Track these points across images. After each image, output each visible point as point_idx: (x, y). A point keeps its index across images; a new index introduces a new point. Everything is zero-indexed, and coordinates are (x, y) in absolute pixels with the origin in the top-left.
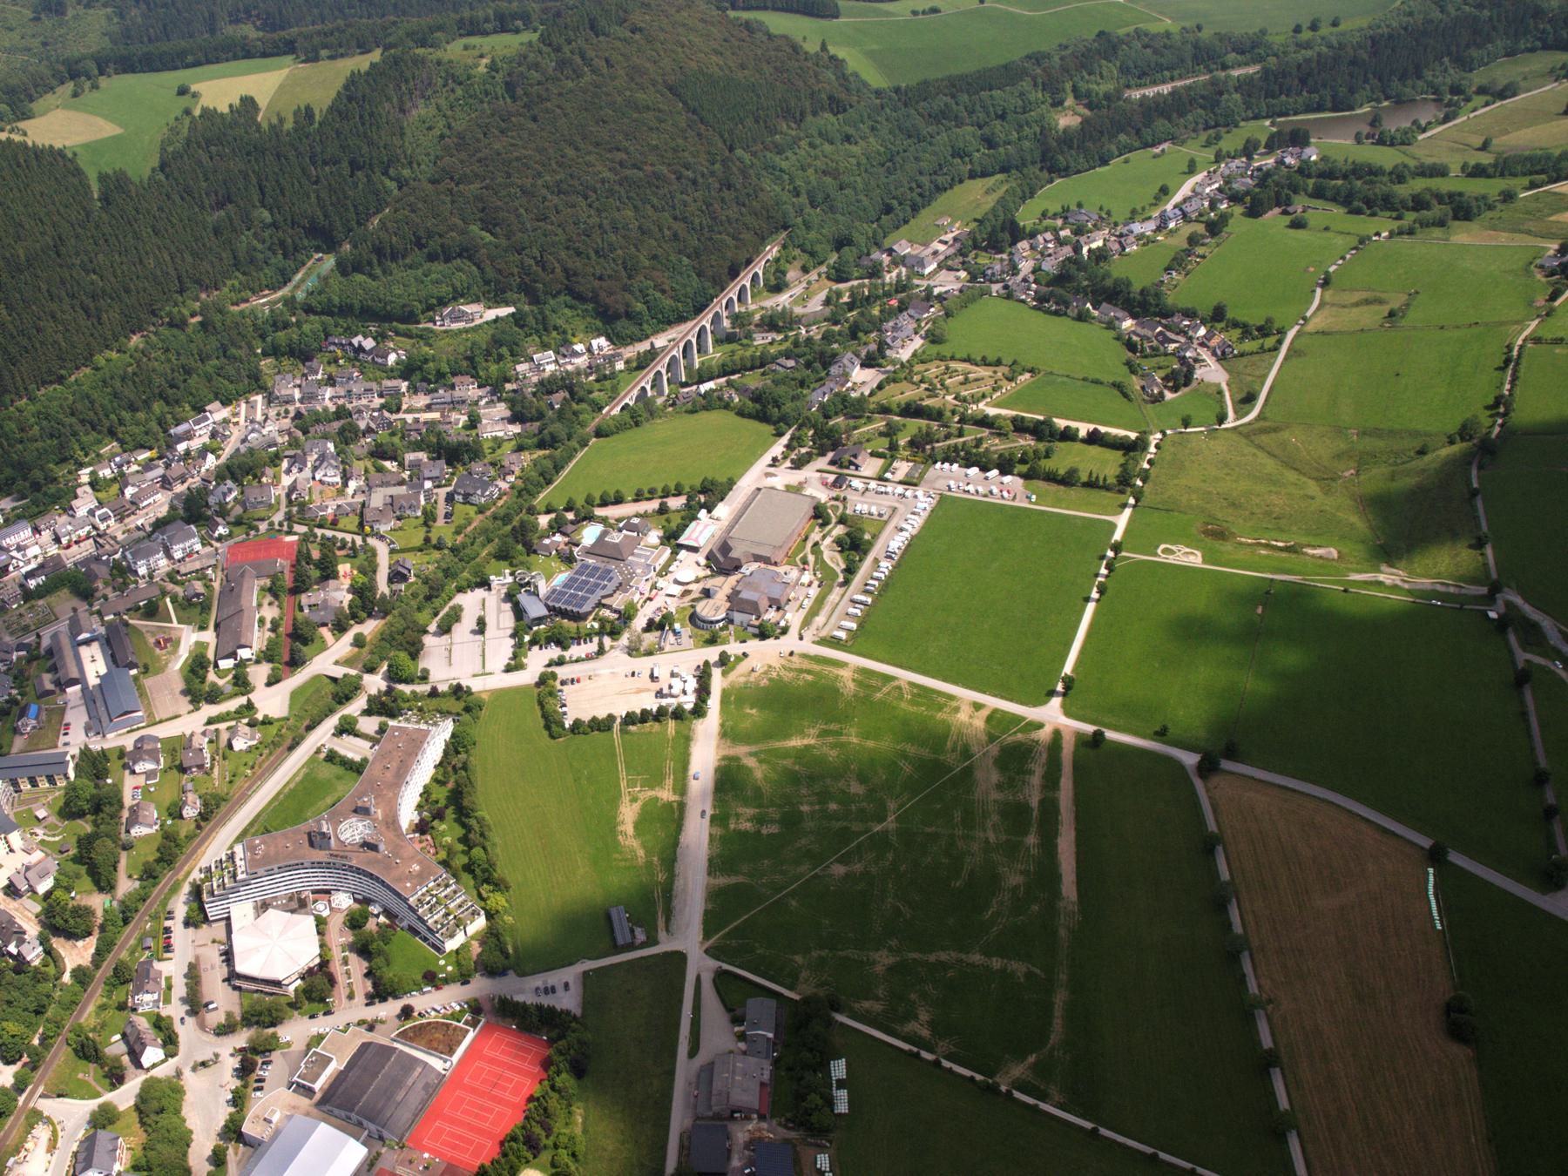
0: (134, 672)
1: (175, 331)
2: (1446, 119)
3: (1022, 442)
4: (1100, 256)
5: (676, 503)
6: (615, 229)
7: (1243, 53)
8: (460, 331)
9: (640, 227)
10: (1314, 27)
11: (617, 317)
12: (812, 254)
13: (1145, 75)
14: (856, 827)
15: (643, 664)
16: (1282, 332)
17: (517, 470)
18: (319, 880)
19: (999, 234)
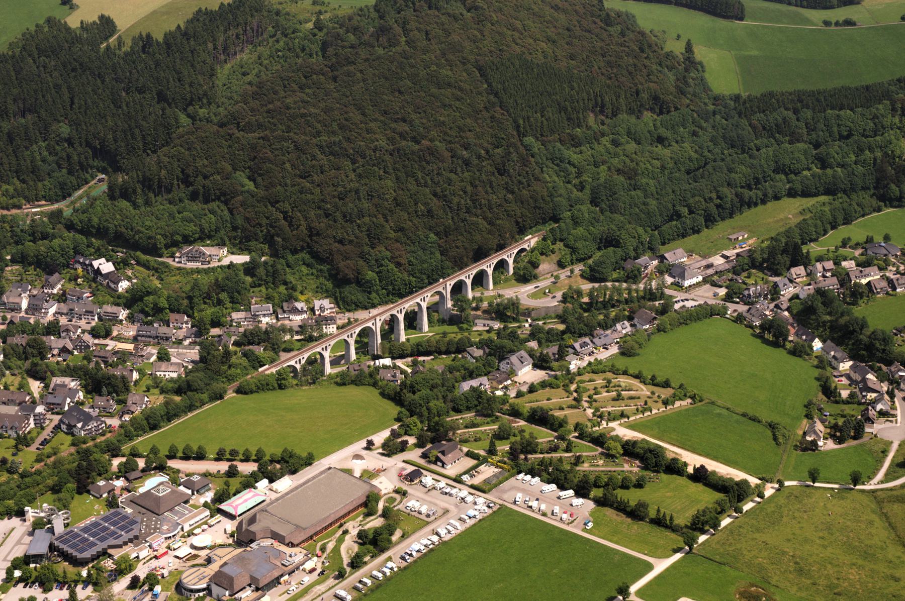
3: (627, 467)
4: (857, 294)
6: (370, 197)
9: (395, 199)
12: (574, 250)
17: (138, 410)
19: (783, 255)
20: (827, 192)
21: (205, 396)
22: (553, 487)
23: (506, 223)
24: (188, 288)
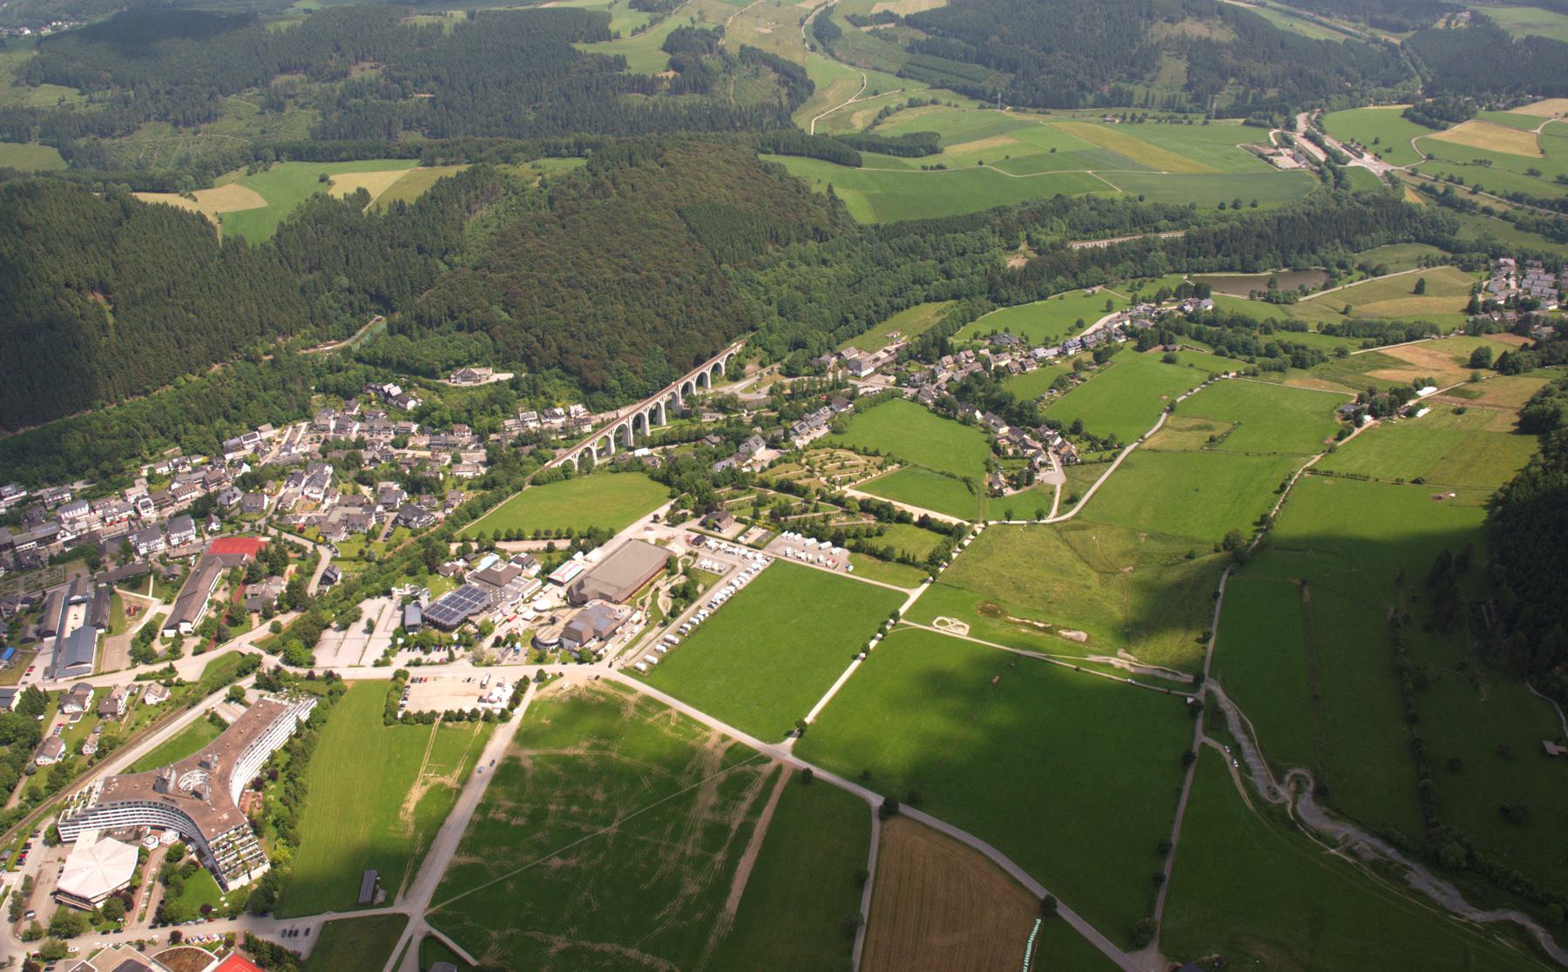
0: (102, 631)
1: (249, 364)
2: (1325, 287)
3: (865, 521)
4: (1000, 373)
5: (562, 544)
7: (1173, 220)
8: (467, 389)
10: (1236, 206)
11: (595, 389)
12: (771, 353)
13: (1088, 231)
14: (584, 828)
15: (480, 673)
16: (1121, 447)
17: (456, 504)
18: (156, 818)
19: (933, 348)
20: (955, 297)
21: (508, 489)
22: (813, 540)
23: (716, 334)
24: (465, 403)
